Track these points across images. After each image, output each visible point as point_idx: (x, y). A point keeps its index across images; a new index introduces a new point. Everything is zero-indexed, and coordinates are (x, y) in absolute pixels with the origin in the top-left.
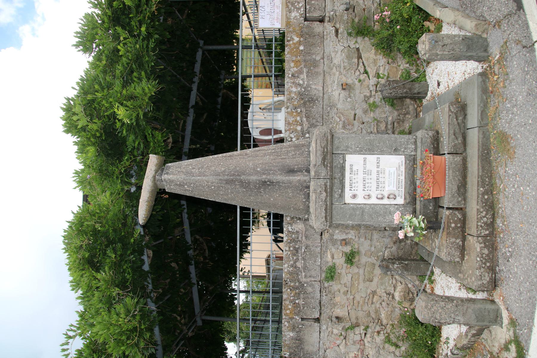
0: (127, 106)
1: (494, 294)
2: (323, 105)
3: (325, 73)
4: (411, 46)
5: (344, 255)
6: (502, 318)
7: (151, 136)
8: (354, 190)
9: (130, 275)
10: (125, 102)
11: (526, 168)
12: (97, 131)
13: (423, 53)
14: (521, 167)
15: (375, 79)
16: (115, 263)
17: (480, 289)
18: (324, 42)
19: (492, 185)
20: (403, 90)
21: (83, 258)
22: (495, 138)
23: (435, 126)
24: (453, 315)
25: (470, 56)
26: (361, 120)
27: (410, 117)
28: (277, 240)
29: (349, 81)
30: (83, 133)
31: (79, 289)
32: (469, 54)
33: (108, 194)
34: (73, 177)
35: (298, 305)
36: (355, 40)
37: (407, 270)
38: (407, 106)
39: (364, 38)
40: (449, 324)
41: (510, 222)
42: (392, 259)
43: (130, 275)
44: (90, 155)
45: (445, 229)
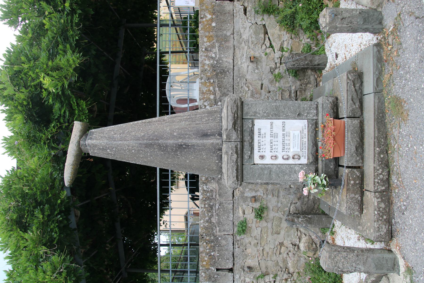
0: (52, 76)
1: (391, 244)
2: (233, 76)
3: (235, 47)
4: (311, 22)
5: (254, 211)
6: (398, 266)
7: (76, 104)
8: (262, 152)
9: (56, 234)
10: (50, 72)
11: (419, 129)
12: (24, 100)
13: (324, 25)
14: (414, 128)
15: (280, 53)
16: (43, 223)
17: (378, 240)
18: (233, 19)
19: (387, 145)
20: (305, 62)
21: (11, 220)
22: (390, 103)
23: (335, 93)
24: (354, 264)
25: (366, 28)
26: (267, 89)
27: (311, 86)
28: (194, 199)
29: (257, 55)
30: (10, 102)
31: (7, 249)
32: (365, 27)
33: (36, 158)
34: (2, 143)
35: (213, 257)
36: (261, 17)
37: (310, 223)
38: (308, 76)
39: (270, 15)
40: (351, 272)
41: (404, 178)
42: (297, 214)
43: (56, 234)
44: (17, 122)
45: (345, 186)
